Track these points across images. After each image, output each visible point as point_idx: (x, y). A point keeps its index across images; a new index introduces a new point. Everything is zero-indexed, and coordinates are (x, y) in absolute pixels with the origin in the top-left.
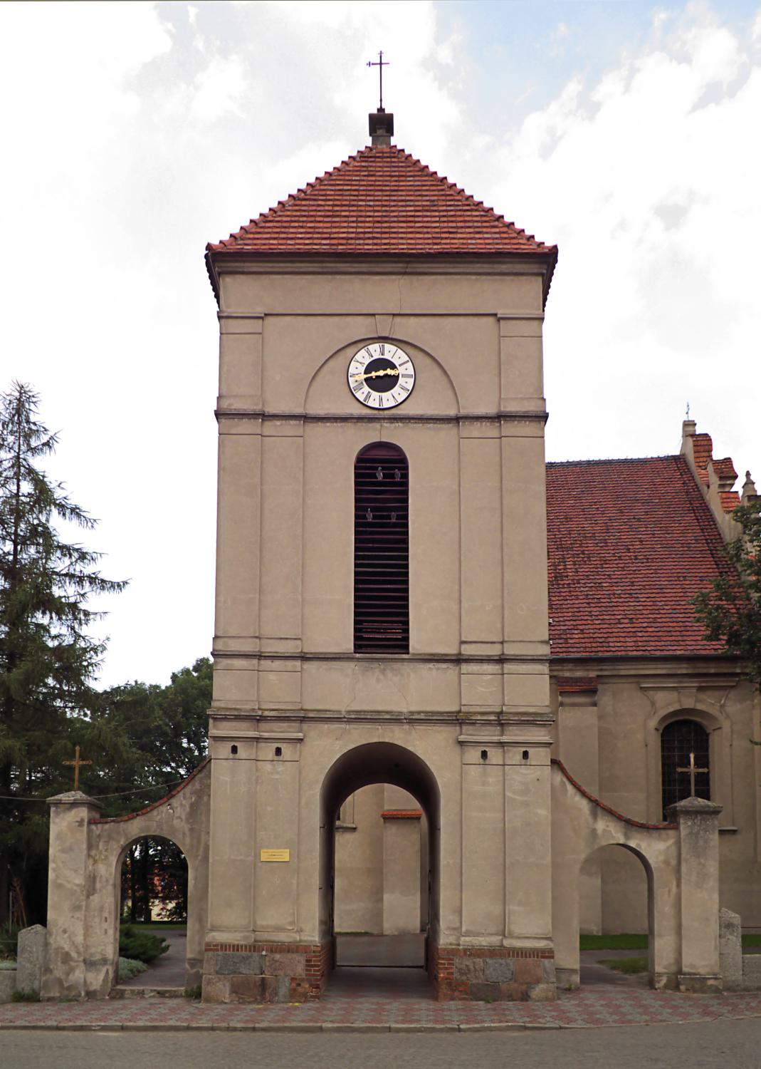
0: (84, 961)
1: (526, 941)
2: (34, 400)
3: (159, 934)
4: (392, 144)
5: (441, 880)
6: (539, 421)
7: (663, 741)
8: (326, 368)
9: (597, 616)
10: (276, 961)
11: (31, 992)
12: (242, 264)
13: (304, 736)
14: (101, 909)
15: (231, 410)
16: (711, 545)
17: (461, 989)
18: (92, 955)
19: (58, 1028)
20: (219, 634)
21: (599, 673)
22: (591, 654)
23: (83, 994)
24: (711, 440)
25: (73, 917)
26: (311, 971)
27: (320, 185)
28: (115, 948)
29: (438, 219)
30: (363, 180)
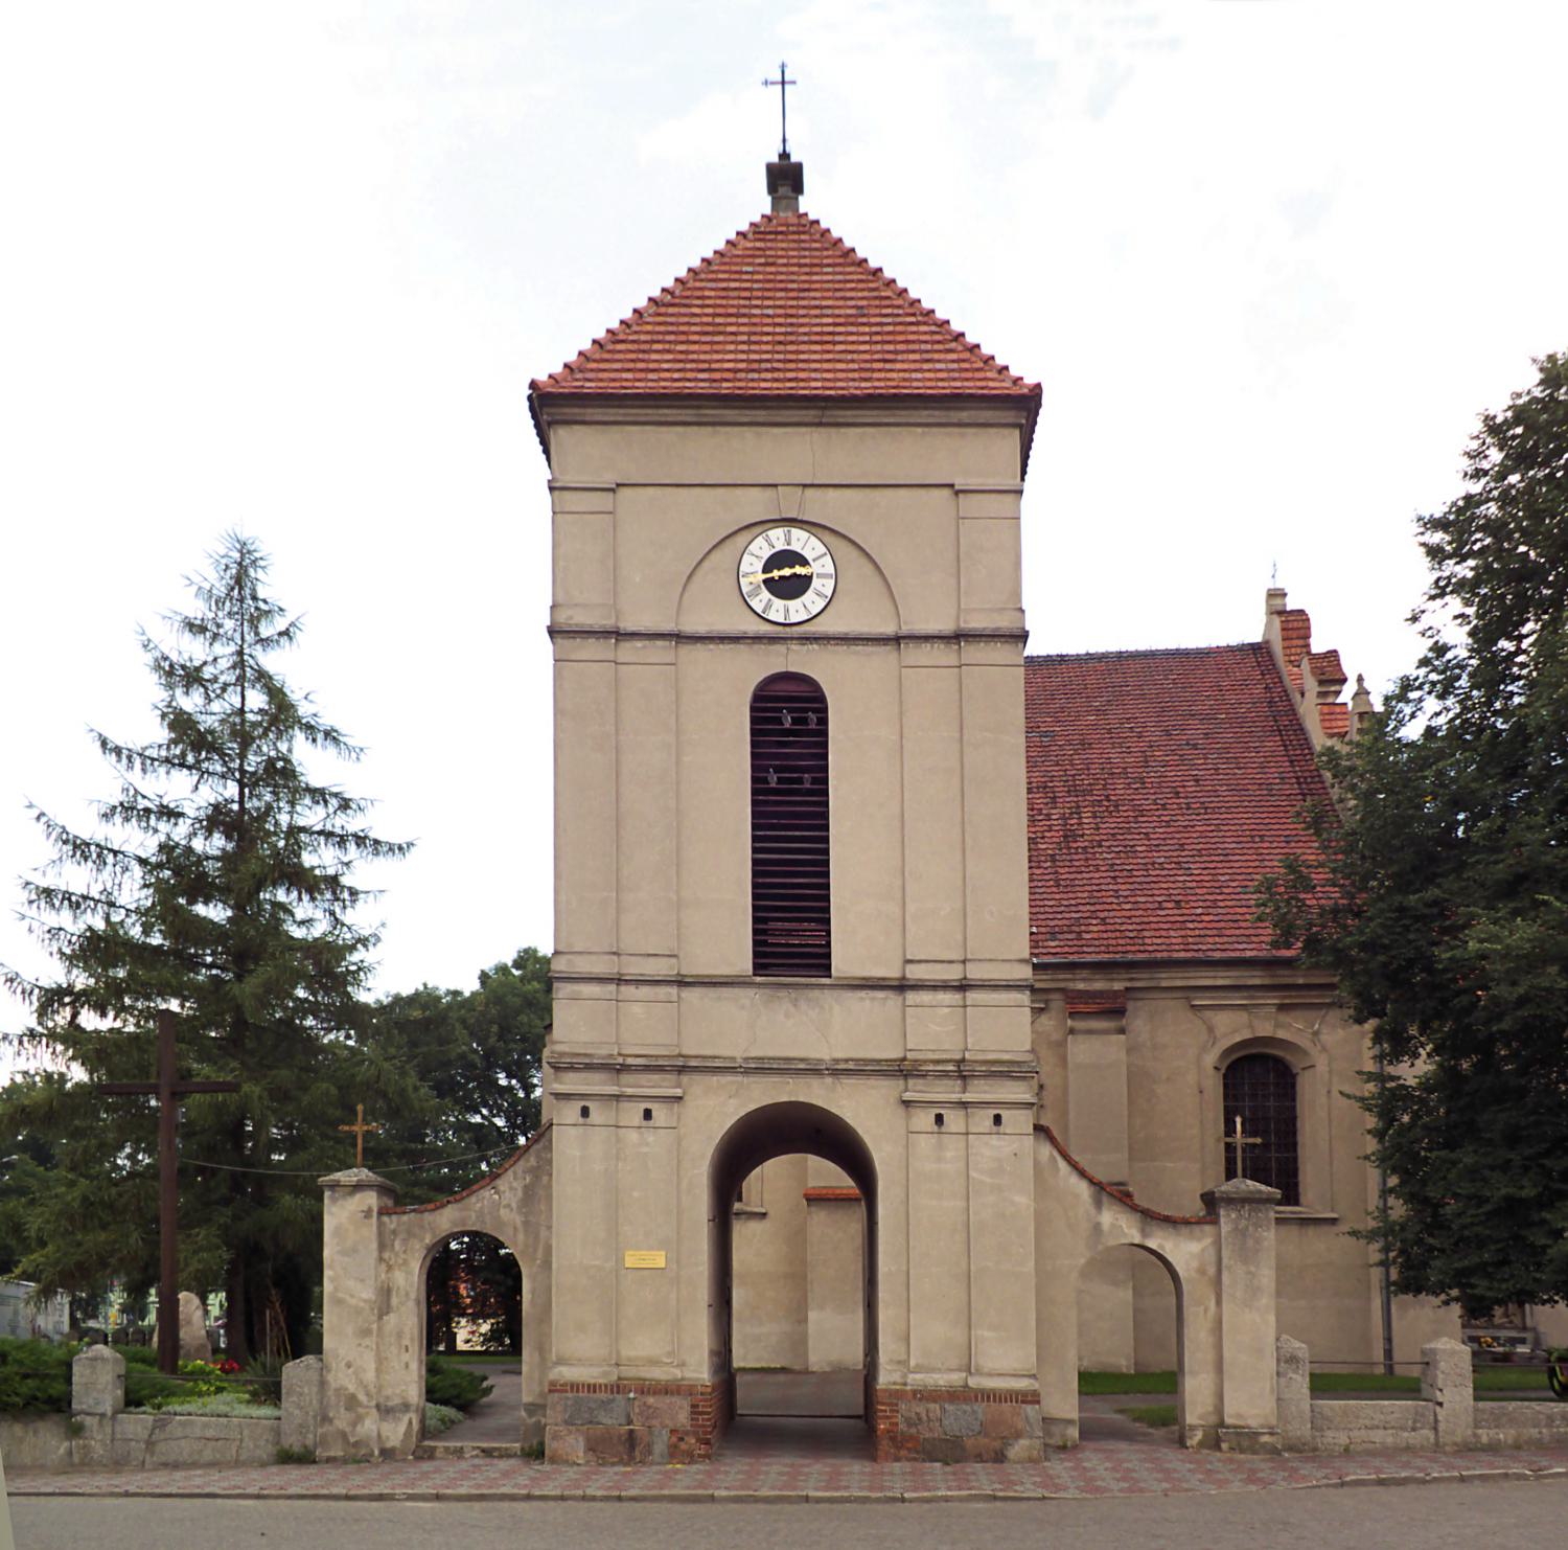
0: (378, 1406)
1: (1001, 1379)
2: (262, 563)
3: (478, 1370)
4: (801, 211)
5: (880, 1295)
6: (1016, 643)
7: (1226, 1086)
8: (706, 564)
9: (1126, 897)
10: (649, 1407)
11: (302, 1450)
12: (582, 411)
13: (684, 1093)
14: (400, 1335)
15: (570, 625)
16: (1304, 786)
17: (910, 1445)
18: (388, 1398)
19: (348, 1498)
20: (560, 949)
21: (1129, 984)
22: (1117, 956)
23: (376, 1452)
24: (1308, 620)
25: (360, 1345)
26: (698, 1420)
27: (695, 280)
28: (420, 1389)
29: (867, 338)
30: (759, 273)
